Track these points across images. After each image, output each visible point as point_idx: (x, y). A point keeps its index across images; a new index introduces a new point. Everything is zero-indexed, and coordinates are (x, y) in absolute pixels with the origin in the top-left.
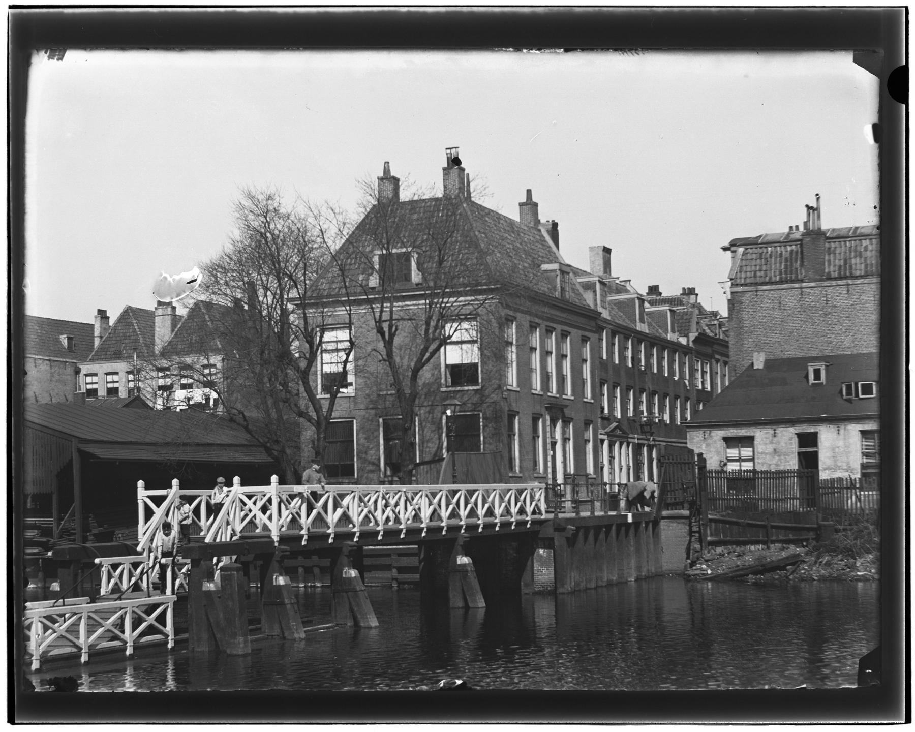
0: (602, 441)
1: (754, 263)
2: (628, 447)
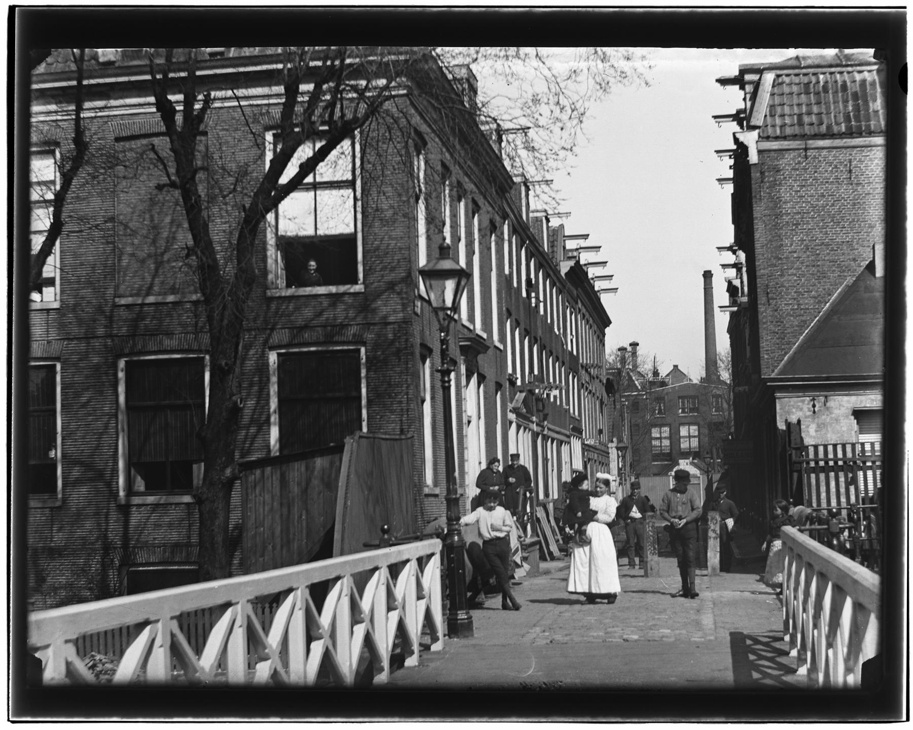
0: (511, 423)
1: (795, 100)
2: (552, 443)
